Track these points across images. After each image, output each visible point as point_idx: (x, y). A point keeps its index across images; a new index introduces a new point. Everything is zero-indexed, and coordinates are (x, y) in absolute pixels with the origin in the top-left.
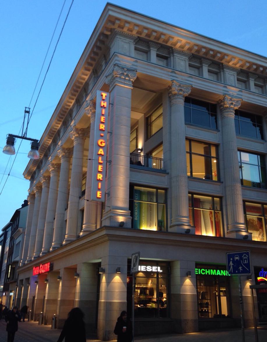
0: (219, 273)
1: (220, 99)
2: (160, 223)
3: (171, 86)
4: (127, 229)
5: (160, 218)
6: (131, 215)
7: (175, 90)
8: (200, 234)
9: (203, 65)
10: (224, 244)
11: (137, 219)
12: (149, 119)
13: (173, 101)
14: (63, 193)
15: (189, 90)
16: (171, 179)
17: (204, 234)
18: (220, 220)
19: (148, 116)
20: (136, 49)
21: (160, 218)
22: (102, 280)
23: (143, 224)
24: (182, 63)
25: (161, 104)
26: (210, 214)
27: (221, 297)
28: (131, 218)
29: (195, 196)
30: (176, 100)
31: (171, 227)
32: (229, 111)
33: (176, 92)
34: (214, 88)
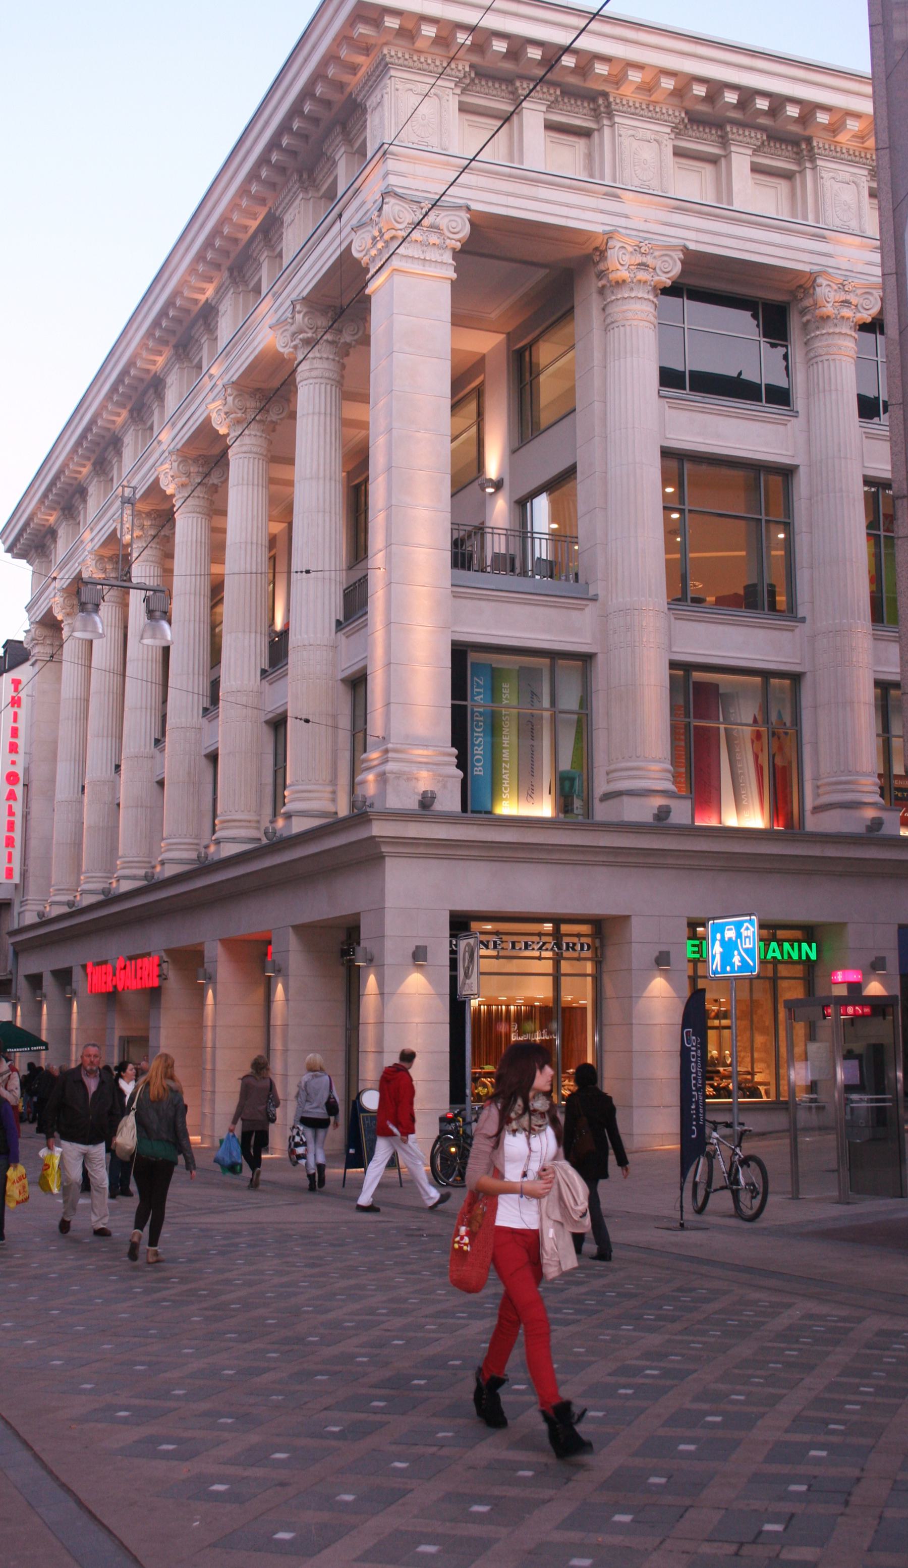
0: (774, 951)
1: (802, 282)
2: (567, 784)
3: (603, 248)
4: (446, 818)
5: (565, 765)
6: (458, 766)
7: (620, 267)
8: (713, 823)
9: (733, 148)
10: (811, 853)
11: (482, 773)
12: (527, 354)
13: (614, 309)
14: (196, 696)
15: (675, 261)
16: (604, 617)
17: (731, 820)
18: (790, 763)
19: (525, 345)
20: (464, 109)
21: (565, 765)
22: (365, 985)
23: (506, 789)
24: (648, 153)
25: (564, 310)
26: (753, 742)
27: (699, 980)
28: (460, 774)
29: (697, 676)
30: (625, 308)
31: (817, 809)
32: (834, 333)
33: (623, 274)
34: (774, 245)
